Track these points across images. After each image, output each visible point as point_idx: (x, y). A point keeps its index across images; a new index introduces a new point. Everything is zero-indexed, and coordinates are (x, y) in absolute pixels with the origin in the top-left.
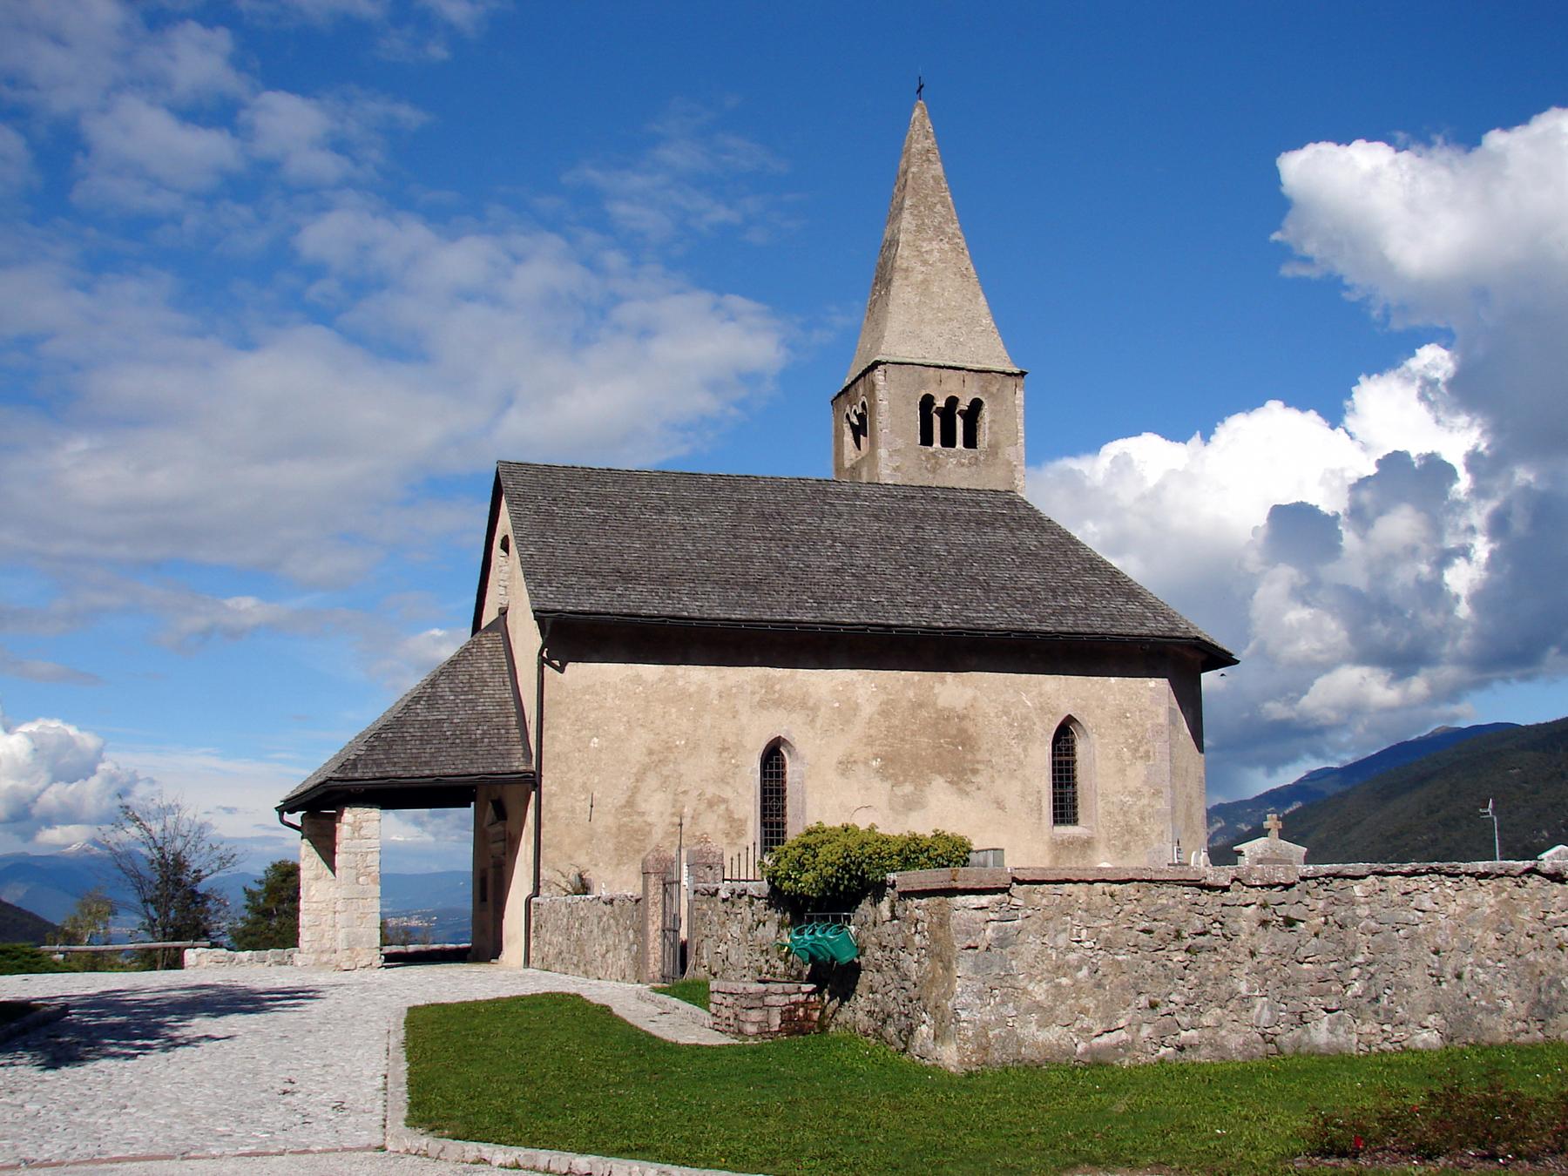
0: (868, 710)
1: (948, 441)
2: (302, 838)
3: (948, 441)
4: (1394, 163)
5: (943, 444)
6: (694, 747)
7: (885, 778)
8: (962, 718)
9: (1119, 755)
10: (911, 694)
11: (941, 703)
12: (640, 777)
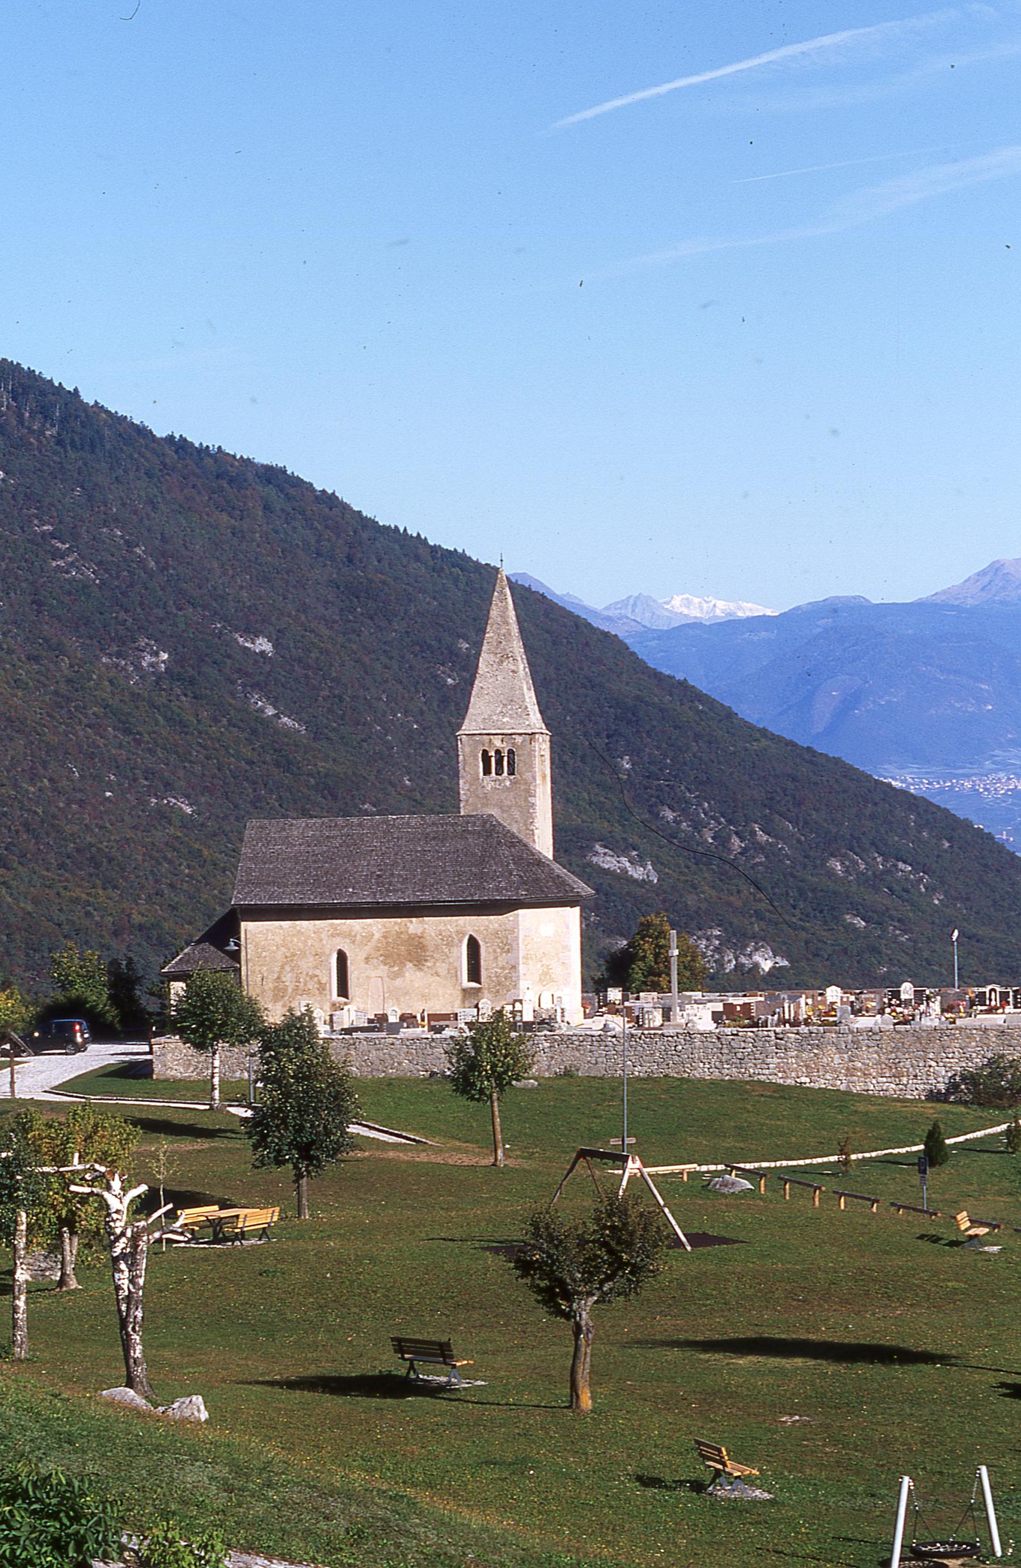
0: (377, 936)
1: (499, 772)
2: (419, 534)
3: (499, 772)
4: (463, 777)
5: (497, 774)
6: (303, 954)
7: (385, 964)
8: (420, 937)
9: (495, 951)
10: (397, 928)
11: (411, 931)
12: (282, 967)
